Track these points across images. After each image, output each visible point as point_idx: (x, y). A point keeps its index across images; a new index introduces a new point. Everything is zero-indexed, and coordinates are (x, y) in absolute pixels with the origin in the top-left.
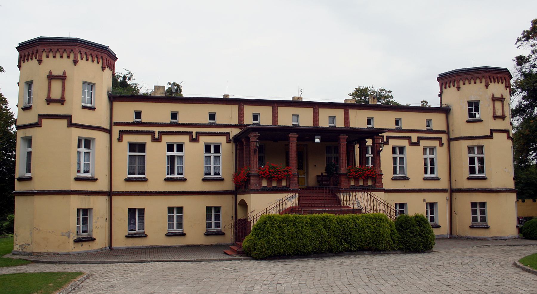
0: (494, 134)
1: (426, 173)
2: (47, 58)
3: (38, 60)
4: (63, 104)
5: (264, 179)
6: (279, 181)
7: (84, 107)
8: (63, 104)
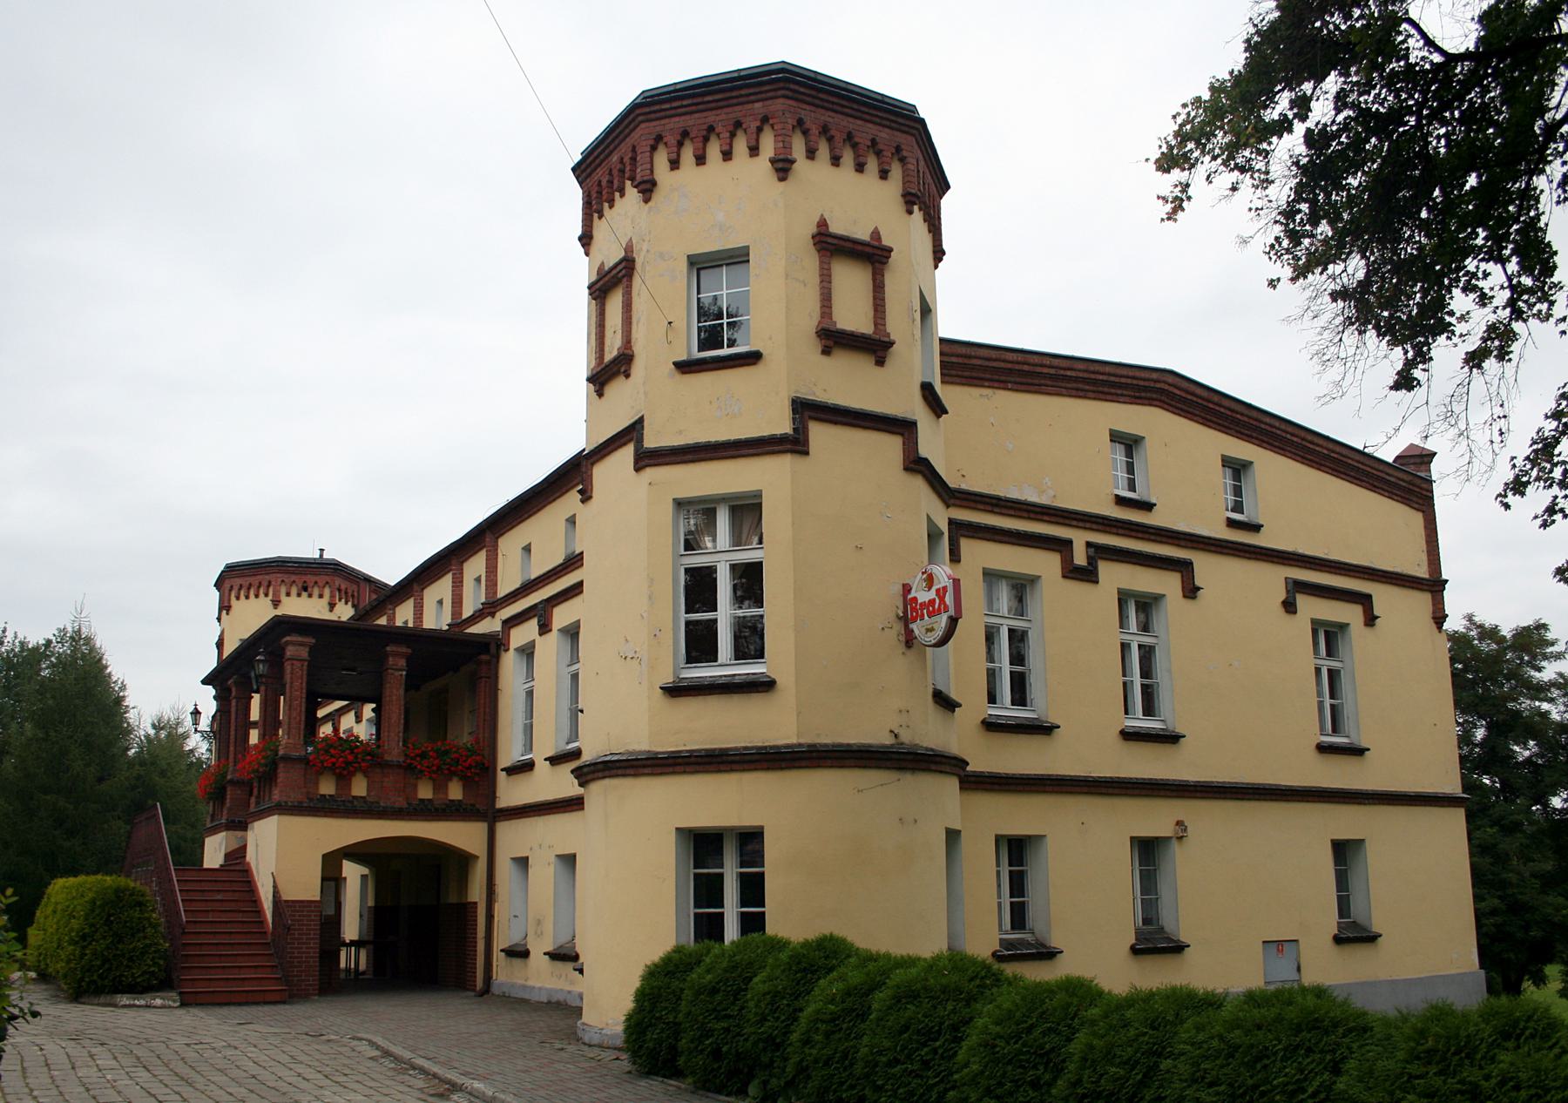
0: (782, 425)
1: (992, 699)
2: (725, 160)
3: (272, 601)
4: (880, 362)
5: (455, 779)
6: (344, 779)
7: (685, 367)
8: (880, 362)
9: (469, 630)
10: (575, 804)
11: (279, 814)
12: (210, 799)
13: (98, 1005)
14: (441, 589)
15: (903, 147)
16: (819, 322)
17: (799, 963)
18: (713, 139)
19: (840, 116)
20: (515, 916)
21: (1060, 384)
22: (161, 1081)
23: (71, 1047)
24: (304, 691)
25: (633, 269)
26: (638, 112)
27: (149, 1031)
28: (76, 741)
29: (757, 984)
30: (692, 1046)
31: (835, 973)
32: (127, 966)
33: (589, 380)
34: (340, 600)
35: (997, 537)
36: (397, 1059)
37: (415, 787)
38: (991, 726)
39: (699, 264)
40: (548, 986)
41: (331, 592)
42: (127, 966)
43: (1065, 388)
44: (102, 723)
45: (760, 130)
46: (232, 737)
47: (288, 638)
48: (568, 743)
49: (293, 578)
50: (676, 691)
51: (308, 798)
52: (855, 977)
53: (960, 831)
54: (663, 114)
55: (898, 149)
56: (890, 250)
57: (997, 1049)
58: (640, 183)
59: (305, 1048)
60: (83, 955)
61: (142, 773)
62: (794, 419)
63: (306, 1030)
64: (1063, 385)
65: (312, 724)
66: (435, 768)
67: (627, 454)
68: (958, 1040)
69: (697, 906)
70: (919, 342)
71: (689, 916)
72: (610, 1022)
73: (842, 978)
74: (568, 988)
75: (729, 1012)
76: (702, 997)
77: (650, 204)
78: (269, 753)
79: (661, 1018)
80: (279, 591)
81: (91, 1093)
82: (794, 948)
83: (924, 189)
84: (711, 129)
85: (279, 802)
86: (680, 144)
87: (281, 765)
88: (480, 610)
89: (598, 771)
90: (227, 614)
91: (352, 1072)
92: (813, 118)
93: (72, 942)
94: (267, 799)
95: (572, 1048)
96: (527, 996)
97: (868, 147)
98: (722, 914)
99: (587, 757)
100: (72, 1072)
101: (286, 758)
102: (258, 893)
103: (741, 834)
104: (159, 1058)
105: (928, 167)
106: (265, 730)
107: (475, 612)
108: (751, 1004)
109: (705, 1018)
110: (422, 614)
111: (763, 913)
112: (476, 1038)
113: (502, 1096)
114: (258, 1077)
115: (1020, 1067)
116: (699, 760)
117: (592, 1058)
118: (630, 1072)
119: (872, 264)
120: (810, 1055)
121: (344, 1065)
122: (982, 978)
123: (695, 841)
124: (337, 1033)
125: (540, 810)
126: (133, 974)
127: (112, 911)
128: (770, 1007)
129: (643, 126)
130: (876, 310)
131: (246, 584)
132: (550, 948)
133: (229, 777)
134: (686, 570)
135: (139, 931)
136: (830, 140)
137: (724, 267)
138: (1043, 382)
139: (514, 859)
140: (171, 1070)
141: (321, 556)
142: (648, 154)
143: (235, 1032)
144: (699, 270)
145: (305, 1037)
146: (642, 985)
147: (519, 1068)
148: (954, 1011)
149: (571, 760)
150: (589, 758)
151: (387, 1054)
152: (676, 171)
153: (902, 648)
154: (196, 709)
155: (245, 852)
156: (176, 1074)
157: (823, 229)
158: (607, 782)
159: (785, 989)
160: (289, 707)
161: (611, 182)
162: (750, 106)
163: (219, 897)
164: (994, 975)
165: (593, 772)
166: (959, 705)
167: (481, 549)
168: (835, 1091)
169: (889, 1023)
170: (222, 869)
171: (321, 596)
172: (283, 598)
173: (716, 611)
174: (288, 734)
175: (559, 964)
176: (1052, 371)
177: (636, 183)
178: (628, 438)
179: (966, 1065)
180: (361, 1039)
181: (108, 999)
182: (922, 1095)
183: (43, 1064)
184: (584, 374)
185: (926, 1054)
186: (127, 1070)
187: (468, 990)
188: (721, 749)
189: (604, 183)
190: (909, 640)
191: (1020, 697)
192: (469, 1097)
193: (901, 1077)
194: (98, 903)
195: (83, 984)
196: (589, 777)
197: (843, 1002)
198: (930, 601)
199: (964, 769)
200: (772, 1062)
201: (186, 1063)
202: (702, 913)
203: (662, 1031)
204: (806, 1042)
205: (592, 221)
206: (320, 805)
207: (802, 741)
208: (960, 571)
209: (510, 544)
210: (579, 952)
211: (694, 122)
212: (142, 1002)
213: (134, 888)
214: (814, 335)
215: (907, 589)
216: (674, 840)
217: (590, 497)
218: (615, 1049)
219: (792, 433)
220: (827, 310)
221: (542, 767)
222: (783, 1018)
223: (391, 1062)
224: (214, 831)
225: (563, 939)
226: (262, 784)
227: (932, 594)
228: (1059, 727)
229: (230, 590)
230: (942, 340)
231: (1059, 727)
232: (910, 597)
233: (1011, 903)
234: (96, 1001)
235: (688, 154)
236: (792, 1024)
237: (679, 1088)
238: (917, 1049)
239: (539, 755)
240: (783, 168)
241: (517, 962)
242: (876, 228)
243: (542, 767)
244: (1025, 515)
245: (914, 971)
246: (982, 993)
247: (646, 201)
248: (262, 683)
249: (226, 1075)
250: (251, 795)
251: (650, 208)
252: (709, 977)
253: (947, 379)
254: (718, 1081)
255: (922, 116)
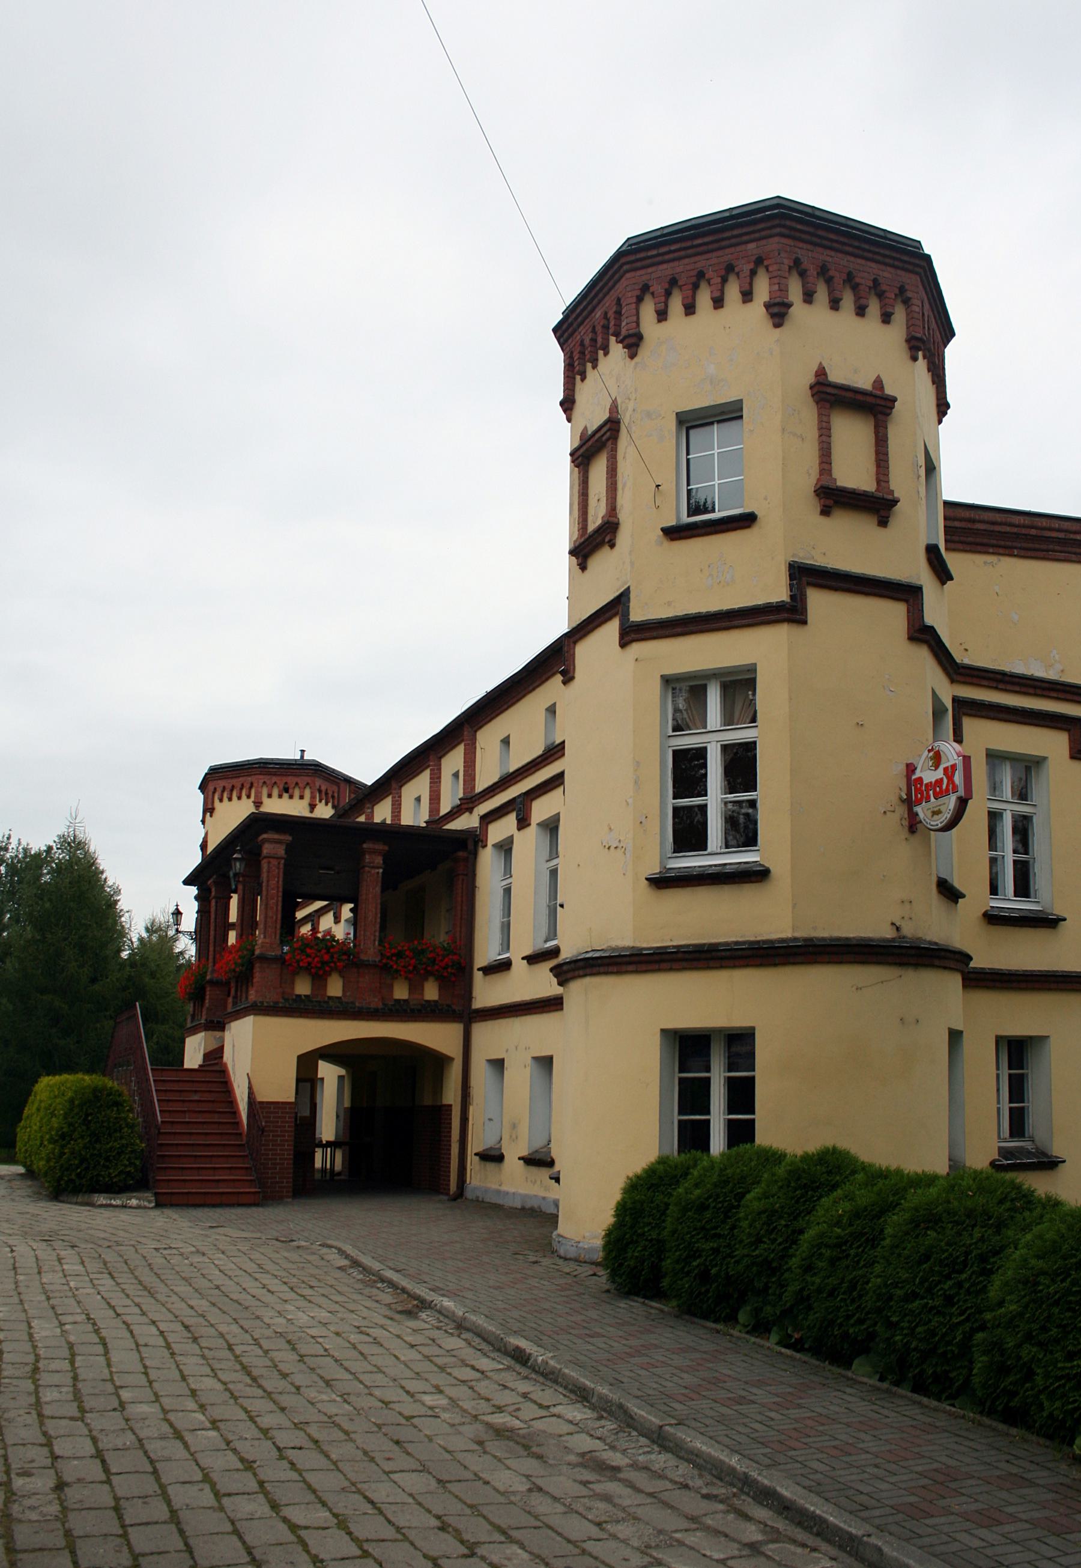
0: (780, 593)
1: (994, 890)
3: (254, 802)
4: (883, 523)
6: (319, 979)
7: (674, 533)
8: (883, 523)
9: (447, 827)
10: (553, 1004)
11: (255, 1014)
12: (190, 999)
13: (76, 1203)
14: (419, 786)
15: (907, 287)
16: (818, 480)
17: (798, 1179)
18: (703, 285)
19: (840, 255)
20: (490, 1120)
21: (1070, 549)
22: (123, 1290)
23: (44, 1252)
24: (281, 889)
25: (618, 431)
26: (623, 261)
27: (122, 1234)
28: (71, 943)
29: (751, 1201)
30: (678, 1267)
31: (839, 1191)
32: (104, 1166)
33: (572, 553)
34: (320, 801)
35: (1001, 716)
36: (365, 1270)
37: (391, 988)
38: (993, 919)
39: (688, 422)
40: (522, 1191)
41: (312, 793)
42: (104, 1166)
43: (1075, 553)
44: (95, 925)
45: (753, 273)
46: (212, 937)
47: (265, 836)
48: (546, 941)
49: (274, 779)
50: (662, 882)
51: (283, 998)
52: (864, 1198)
53: (962, 1032)
54: (649, 261)
55: (902, 290)
56: (894, 400)
57: (1041, 1288)
58: (625, 337)
59: (275, 1256)
60: (62, 1154)
61: (133, 974)
62: (791, 586)
63: (275, 1234)
64: (1074, 550)
65: (289, 925)
66: (411, 968)
67: (611, 629)
68: (988, 1273)
69: (680, 1113)
70: (924, 502)
71: (673, 1123)
72: (587, 1234)
73: (849, 1197)
74: (542, 1194)
75: (718, 1231)
76: (689, 1213)
77: (636, 359)
78: (245, 952)
79: (643, 1234)
80: (261, 793)
81: (52, 1302)
82: (792, 1163)
83: (929, 334)
84: (701, 275)
85: (255, 1002)
86: (668, 294)
87: (257, 965)
88: (458, 806)
89: (578, 969)
90: (211, 816)
91: (318, 1284)
92: (810, 257)
93: (52, 1141)
94: (243, 1000)
95: (546, 1262)
96: (500, 1202)
97: (870, 288)
98: (708, 1121)
99: (566, 954)
100: (37, 1277)
101: (263, 958)
102: (234, 1094)
103: (729, 1035)
104: (126, 1263)
105: (933, 311)
106: (242, 930)
107: (453, 808)
108: (745, 1224)
109: (693, 1236)
110: (400, 812)
111: (753, 1120)
112: (448, 1248)
113: (473, 1318)
114: (222, 1288)
115: (1069, 1309)
116: (687, 956)
117: (568, 1274)
118: (608, 1291)
119: (875, 416)
120: (813, 1283)
121: (312, 1276)
122: (1012, 1200)
123: (680, 1042)
124: (307, 1239)
125: (517, 1011)
126: (110, 1174)
127: (90, 1111)
128: (765, 1227)
129: (628, 275)
130: (878, 466)
131: (229, 787)
132: (525, 1153)
133: (208, 977)
134: (674, 752)
135: (116, 1131)
136: (829, 281)
137: (716, 425)
138: (1051, 547)
139: (490, 1061)
140: (136, 1278)
141: (302, 757)
142: (634, 306)
143: (206, 1236)
144: (688, 429)
145: (275, 1242)
146: (623, 1199)
147: (491, 1283)
148: (982, 1239)
149: (550, 959)
150: (569, 955)
151: (356, 1263)
152: (664, 323)
153: (905, 833)
154: (177, 909)
155: (223, 1053)
156: (140, 1283)
157: (821, 379)
158: (588, 981)
159: (782, 1207)
160: (266, 906)
161: (594, 341)
162: (743, 247)
163: (196, 1097)
164: (1024, 1196)
165: (574, 970)
166: (963, 896)
167: (459, 744)
168: (841, 1325)
169: (906, 1252)
170: (201, 1069)
171: (301, 797)
172: (265, 800)
173: (706, 795)
174: (265, 933)
175: (534, 1170)
176: (1061, 535)
177: (621, 338)
178: (613, 611)
179: (1001, 1304)
180: (330, 1247)
181: (86, 1198)
182: (944, 1335)
183: (11, 1267)
184: (566, 547)
185: (950, 1288)
186: (92, 1276)
187: (442, 1193)
188: (711, 945)
189: (587, 342)
190: (913, 825)
191: (1023, 888)
192: (438, 1315)
193: (920, 1314)
194: (77, 1102)
195: (62, 1182)
196: (569, 975)
197: (851, 1225)
198: (937, 781)
199: (967, 965)
200: (766, 1288)
201: (152, 1269)
202: (686, 1121)
203: (645, 1249)
204: (808, 1268)
205: (574, 384)
206: (295, 1006)
207: (797, 935)
208: (964, 749)
209: (488, 737)
210: (554, 1157)
211: (682, 268)
212: (119, 1202)
213: (111, 1088)
214: (813, 494)
215: (911, 769)
216: (658, 1042)
217: (572, 678)
218: (593, 1263)
219: (789, 600)
220: (826, 466)
221: (519, 966)
222: (780, 1240)
223: (361, 1273)
224: (194, 1031)
225: (539, 1143)
226: (239, 984)
227: (939, 774)
228: (1065, 920)
229: (214, 793)
230: (947, 504)
231: (1065, 920)
232: (914, 777)
233: (1011, 1109)
234: (75, 1200)
235: (676, 305)
236: (790, 1247)
237: (662, 1311)
238: (940, 1282)
239: (517, 953)
240: (778, 312)
241: (491, 1166)
242: (878, 376)
243: (519, 966)
244: (1031, 691)
245: (933, 1191)
246: (1012, 1217)
247: (632, 356)
248: (239, 881)
249: (191, 1285)
250: (229, 995)
251: (637, 363)
252: (697, 1192)
253: (953, 546)
254: (705, 1306)
255: (926, 251)
